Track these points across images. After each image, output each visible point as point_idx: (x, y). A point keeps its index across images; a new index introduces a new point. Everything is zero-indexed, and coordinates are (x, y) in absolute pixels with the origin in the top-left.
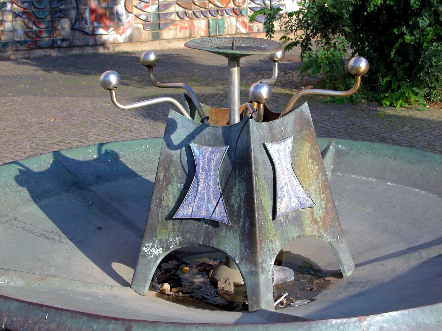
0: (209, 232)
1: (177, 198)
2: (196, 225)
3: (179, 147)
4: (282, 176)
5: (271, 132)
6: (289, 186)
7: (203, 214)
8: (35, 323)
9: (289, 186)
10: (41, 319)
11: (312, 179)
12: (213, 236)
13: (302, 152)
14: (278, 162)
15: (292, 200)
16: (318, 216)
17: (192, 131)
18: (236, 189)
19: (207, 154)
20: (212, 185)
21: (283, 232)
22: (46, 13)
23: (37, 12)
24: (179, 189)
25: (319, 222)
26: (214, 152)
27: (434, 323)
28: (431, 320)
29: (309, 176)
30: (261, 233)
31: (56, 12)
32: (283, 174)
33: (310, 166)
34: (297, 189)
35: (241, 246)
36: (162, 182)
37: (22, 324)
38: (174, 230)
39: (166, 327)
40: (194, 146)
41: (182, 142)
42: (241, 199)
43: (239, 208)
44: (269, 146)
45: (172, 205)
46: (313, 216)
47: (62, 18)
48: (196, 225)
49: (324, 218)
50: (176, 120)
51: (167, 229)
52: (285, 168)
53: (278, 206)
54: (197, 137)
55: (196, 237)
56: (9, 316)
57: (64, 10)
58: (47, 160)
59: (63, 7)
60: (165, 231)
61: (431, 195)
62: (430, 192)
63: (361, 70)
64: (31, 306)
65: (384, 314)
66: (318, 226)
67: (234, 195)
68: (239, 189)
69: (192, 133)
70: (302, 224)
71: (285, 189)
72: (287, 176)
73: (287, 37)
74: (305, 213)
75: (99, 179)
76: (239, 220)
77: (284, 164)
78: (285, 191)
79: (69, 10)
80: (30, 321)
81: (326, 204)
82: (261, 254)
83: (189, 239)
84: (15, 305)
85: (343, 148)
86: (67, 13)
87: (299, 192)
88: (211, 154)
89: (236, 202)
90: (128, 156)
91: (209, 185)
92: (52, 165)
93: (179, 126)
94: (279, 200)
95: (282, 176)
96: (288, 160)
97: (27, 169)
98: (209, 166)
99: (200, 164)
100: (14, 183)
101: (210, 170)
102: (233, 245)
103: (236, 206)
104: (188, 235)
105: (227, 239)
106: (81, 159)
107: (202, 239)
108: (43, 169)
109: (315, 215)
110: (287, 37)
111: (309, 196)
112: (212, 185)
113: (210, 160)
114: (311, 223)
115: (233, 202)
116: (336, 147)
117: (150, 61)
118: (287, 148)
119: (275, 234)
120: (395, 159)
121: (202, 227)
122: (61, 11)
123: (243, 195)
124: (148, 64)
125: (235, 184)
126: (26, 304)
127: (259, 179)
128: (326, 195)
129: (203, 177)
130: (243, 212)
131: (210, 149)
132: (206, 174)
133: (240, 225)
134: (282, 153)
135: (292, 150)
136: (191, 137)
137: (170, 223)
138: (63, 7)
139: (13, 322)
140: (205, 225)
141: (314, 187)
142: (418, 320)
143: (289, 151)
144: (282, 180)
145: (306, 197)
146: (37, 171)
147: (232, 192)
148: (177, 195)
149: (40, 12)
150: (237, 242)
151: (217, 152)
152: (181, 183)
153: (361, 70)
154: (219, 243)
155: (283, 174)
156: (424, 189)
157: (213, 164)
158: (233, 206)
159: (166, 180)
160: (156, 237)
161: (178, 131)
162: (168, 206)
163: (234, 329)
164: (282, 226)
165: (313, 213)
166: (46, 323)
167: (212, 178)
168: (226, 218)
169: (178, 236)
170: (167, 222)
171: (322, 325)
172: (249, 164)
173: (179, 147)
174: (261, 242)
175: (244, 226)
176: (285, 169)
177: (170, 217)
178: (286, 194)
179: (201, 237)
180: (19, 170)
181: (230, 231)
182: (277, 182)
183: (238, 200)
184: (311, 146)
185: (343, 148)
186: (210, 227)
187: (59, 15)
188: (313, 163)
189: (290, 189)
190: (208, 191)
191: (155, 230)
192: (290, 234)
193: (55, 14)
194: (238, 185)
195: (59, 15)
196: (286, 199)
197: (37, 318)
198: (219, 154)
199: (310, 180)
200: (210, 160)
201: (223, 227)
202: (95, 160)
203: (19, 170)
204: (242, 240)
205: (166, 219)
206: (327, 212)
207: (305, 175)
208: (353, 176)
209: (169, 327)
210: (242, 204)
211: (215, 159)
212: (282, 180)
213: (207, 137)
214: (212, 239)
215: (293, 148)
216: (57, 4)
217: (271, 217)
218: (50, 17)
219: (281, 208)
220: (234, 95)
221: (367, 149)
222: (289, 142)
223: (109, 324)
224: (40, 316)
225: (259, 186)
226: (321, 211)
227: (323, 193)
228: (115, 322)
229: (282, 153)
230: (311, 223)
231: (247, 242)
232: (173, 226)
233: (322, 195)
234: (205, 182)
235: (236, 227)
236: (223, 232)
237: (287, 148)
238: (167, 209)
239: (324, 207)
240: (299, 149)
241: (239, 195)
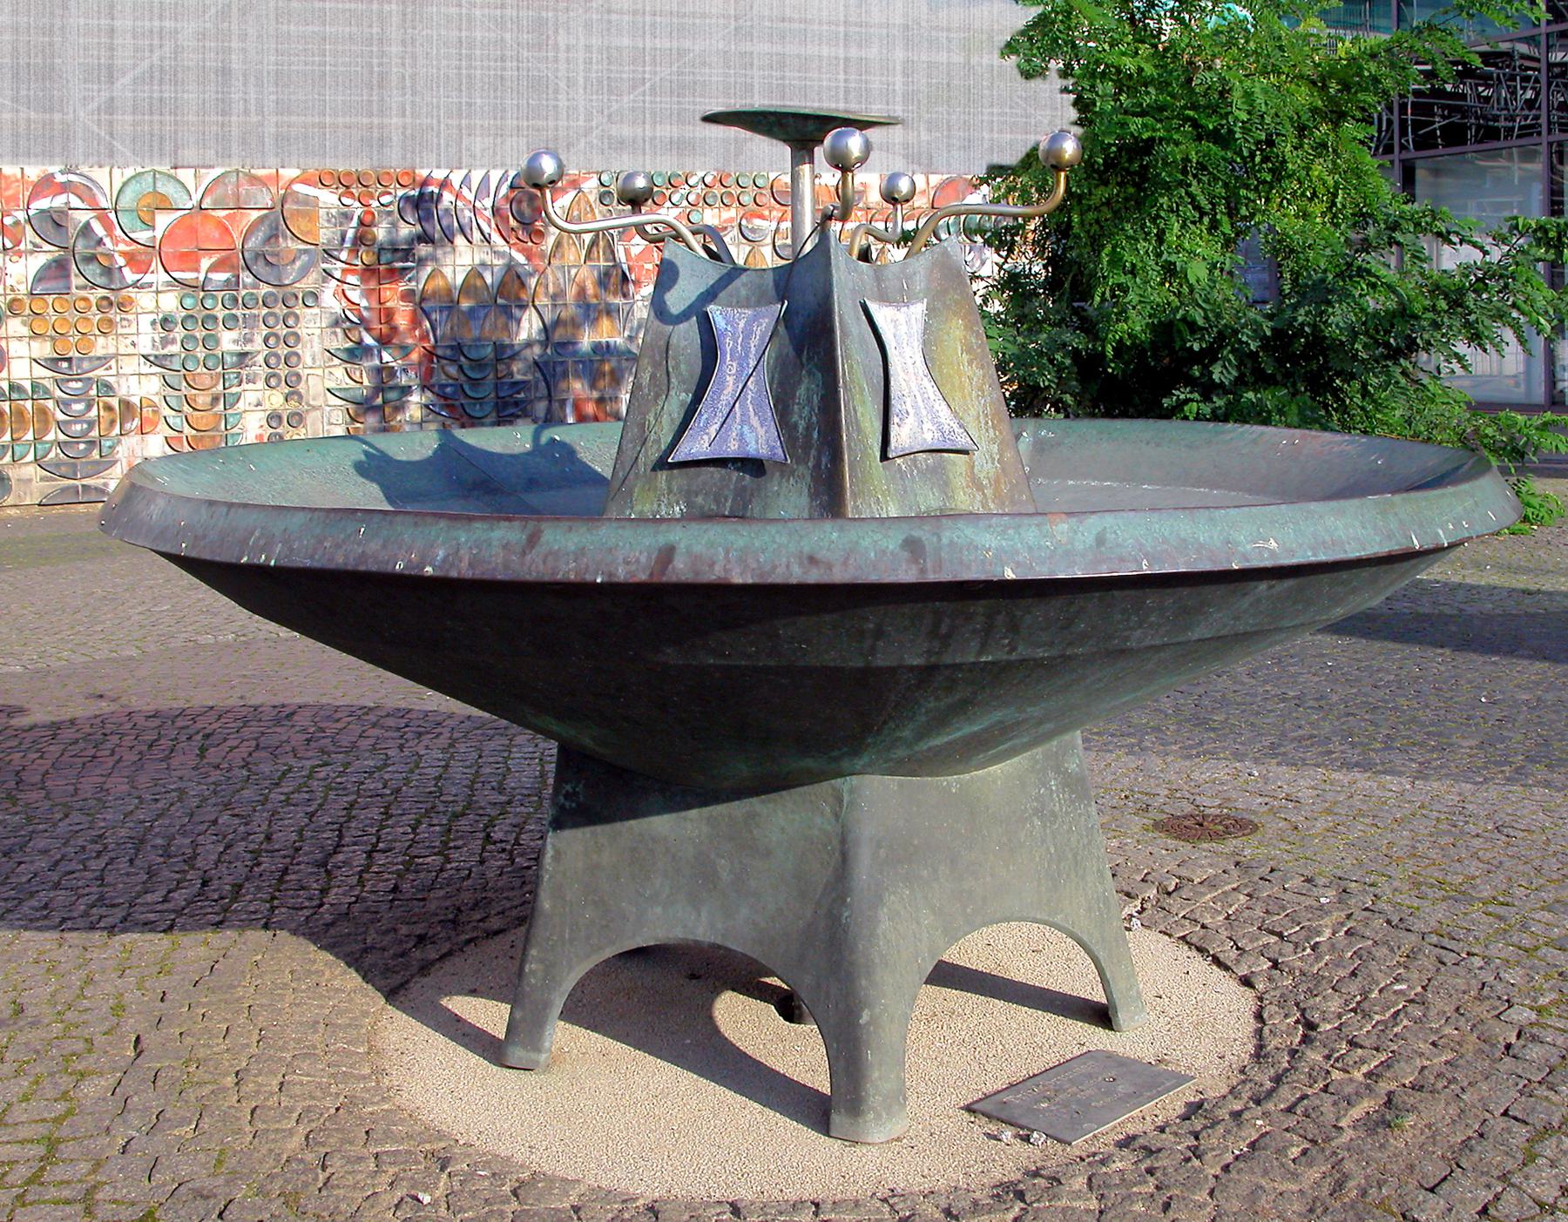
0: (744, 488)
1: (677, 423)
2: (717, 476)
3: (684, 316)
4: (902, 375)
5: (879, 285)
6: (919, 399)
7: (732, 449)
8: (338, 546)
9: (919, 399)
10: (350, 536)
11: (970, 394)
12: (752, 495)
13: (946, 337)
14: (894, 344)
15: (925, 427)
16: (984, 474)
17: (711, 282)
18: (801, 391)
19: (742, 324)
21: (905, 492)
22: (488, 408)
23: (469, 404)
24: (682, 403)
25: (985, 487)
26: (755, 318)
27: (1219, 544)
28: (1212, 538)
29: (962, 388)
30: (856, 476)
31: (506, 405)
32: (905, 371)
33: (965, 368)
34: (936, 407)
35: (811, 507)
36: (646, 391)
37: (310, 551)
38: (670, 491)
39: (617, 528)
40: (713, 310)
41: (690, 307)
43: (808, 428)
44: (873, 307)
45: (666, 439)
46: (972, 473)
47: (518, 417)
48: (717, 476)
49: (997, 481)
50: (678, 263)
51: (656, 489)
52: (910, 362)
53: (894, 431)
54: (722, 295)
55: (717, 502)
56: (285, 542)
57: (522, 401)
58: (426, 442)
59: (522, 395)
60: (651, 494)
61: (1233, 493)
62: (1231, 489)
63: (1067, 156)
64: (332, 515)
66: (983, 493)
67: (799, 404)
68: (808, 389)
69: (712, 286)
70: (947, 484)
71: (908, 400)
72: (913, 378)
74: (954, 464)
75: (532, 483)
76: (807, 454)
77: (908, 351)
78: (908, 404)
79: (531, 401)
80: (327, 544)
81: (1001, 452)
83: (702, 507)
84: (300, 518)
85: (1050, 435)
86: (529, 407)
87: (941, 414)
88: (749, 324)
89: (801, 417)
90: (596, 449)
92: (435, 453)
93: (684, 273)
94: (895, 420)
95: (902, 375)
96: (917, 346)
97: (382, 452)
98: (746, 349)
99: (727, 345)
100: (352, 470)
101: (747, 356)
102: (796, 507)
103: (802, 425)
104: (700, 500)
105: (782, 498)
106: (497, 449)
107: (728, 504)
108: (416, 458)
109: (976, 471)
111: (961, 426)
113: (748, 335)
114: (968, 486)
115: (795, 418)
116: (1035, 434)
117: (635, 190)
118: (913, 321)
119: (888, 490)
120: (1158, 445)
121: (730, 479)
122: (516, 404)
123: (816, 400)
124: (631, 196)
125: (800, 382)
126: (321, 514)
127: (851, 367)
128: (1000, 432)
129: (734, 371)
130: (815, 435)
131: (749, 312)
132: (740, 365)
133: (810, 464)
134: (903, 328)
135: (925, 329)
136: (710, 295)
137: (663, 476)
138: (522, 395)
139: (291, 550)
140: (735, 475)
141: (973, 412)
142: (1183, 534)
143: (917, 328)
144: (904, 384)
145: (956, 427)
146: (404, 458)
147: (794, 396)
148: (678, 416)
149: (475, 405)
150: (804, 500)
151: (764, 317)
152: (686, 392)
153: (1067, 156)
155: (905, 371)
156: (1218, 487)
157: (754, 342)
158: (796, 426)
159: (656, 386)
160: (632, 508)
161: (680, 281)
162: (658, 441)
163: (768, 528)
164: (902, 478)
165: (973, 467)
166: (359, 543)
168: (780, 451)
169: (678, 504)
170: (656, 477)
172: (829, 331)
173: (684, 316)
174: (854, 495)
175: (817, 465)
176: (910, 362)
177: (662, 464)
178: (911, 411)
179: (726, 500)
180: (366, 453)
181: (788, 480)
182: (892, 383)
183: (806, 412)
184: (966, 326)
185: (1050, 435)
186: (747, 476)
187: (511, 410)
188: (970, 363)
189: (921, 404)
191: (630, 493)
192: (920, 499)
193: (504, 410)
194: (806, 381)
195: (511, 410)
196: (911, 421)
197: (342, 536)
199: (964, 397)
200: (748, 335)
201: (773, 474)
202: (528, 454)
203: (366, 453)
204: (813, 495)
205: (654, 469)
206: (1003, 469)
207: (953, 385)
208: (1071, 482)
209: (624, 528)
210: (814, 418)
211: (758, 333)
212: (904, 384)
213: (743, 292)
214: (750, 501)
215: (927, 327)
217: (878, 454)
218: (494, 414)
219: (901, 436)
220: (803, 221)
221: (1100, 433)
222: (918, 309)
223: (493, 530)
224: (349, 532)
225: (852, 381)
226: (990, 464)
227: (994, 427)
228: (507, 523)
229: (903, 328)
230: (968, 486)
231: (825, 498)
232: (669, 481)
233: (991, 431)
235: (801, 469)
236: (773, 484)
237: (913, 321)
238: (656, 447)
239: (997, 457)
240: (941, 330)
241: (809, 400)
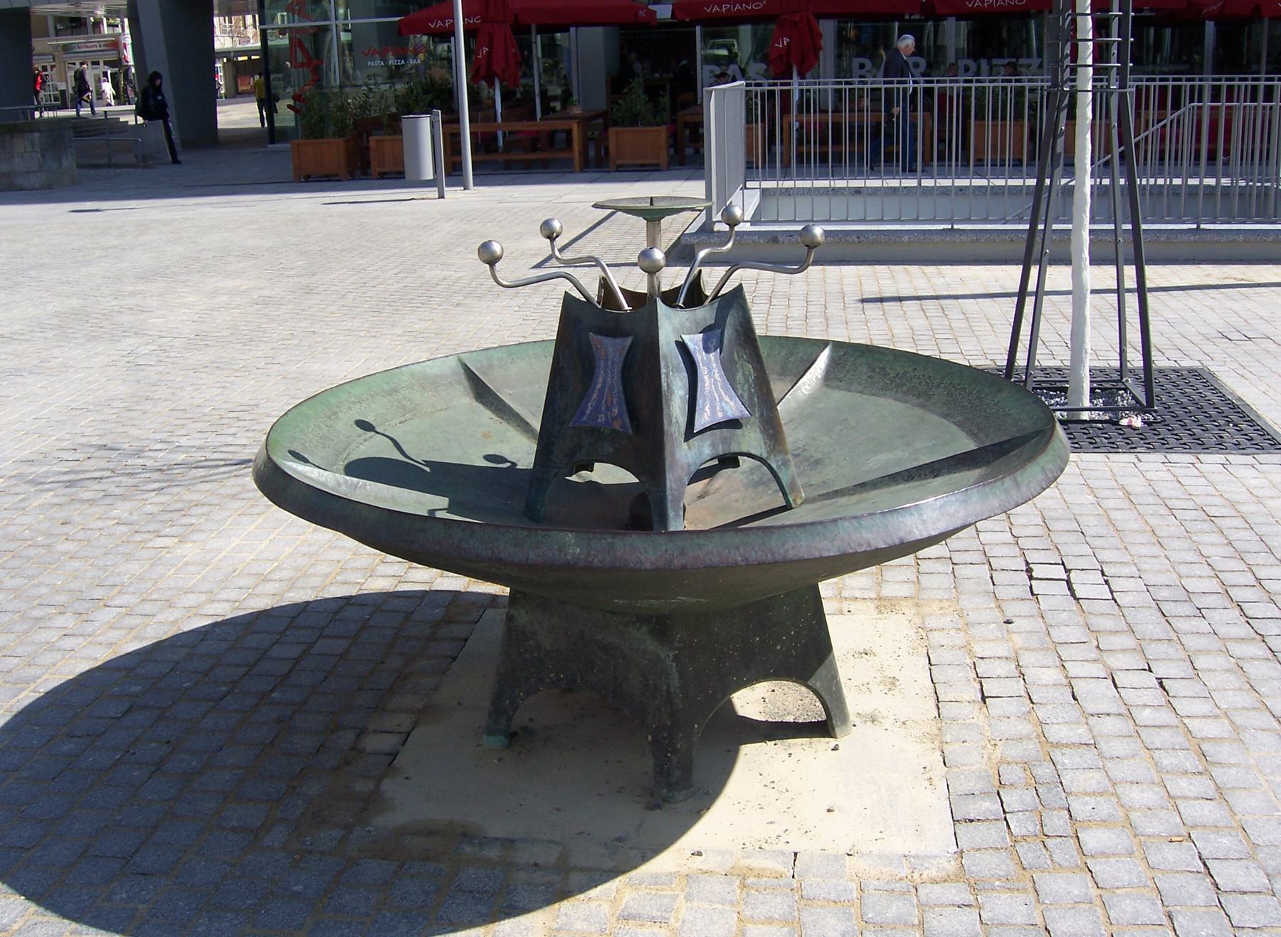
20: (718, 379)
42: (750, 385)
65: (1025, 311)
73: (792, 79)
82: (652, 564)
91: (715, 380)
101: (710, 361)
110: (792, 79)
112: (718, 379)
130: (756, 399)
132: (708, 368)
133: (757, 416)
154: (739, 444)
167: (716, 371)
171: (801, 533)
183: (746, 387)
190: (716, 388)
198: (715, 339)
214: (730, 443)
216: (494, 90)
234: (710, 378)
